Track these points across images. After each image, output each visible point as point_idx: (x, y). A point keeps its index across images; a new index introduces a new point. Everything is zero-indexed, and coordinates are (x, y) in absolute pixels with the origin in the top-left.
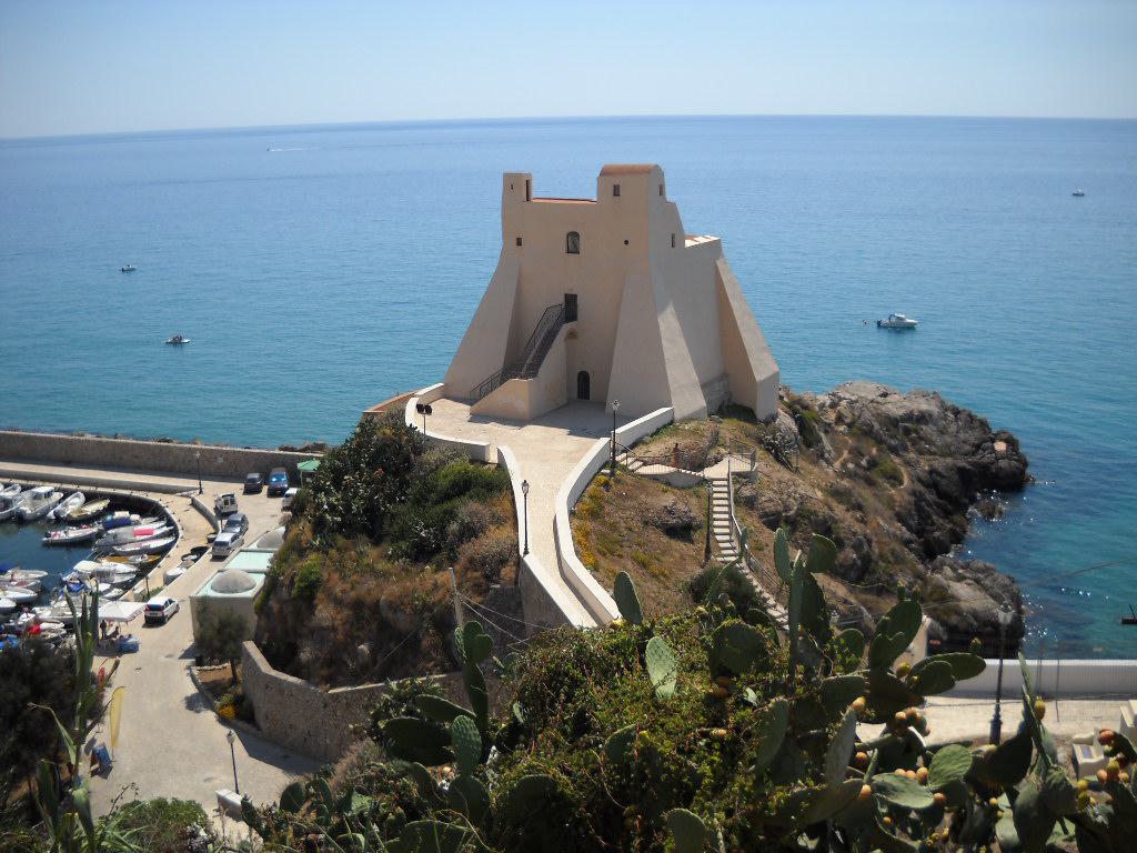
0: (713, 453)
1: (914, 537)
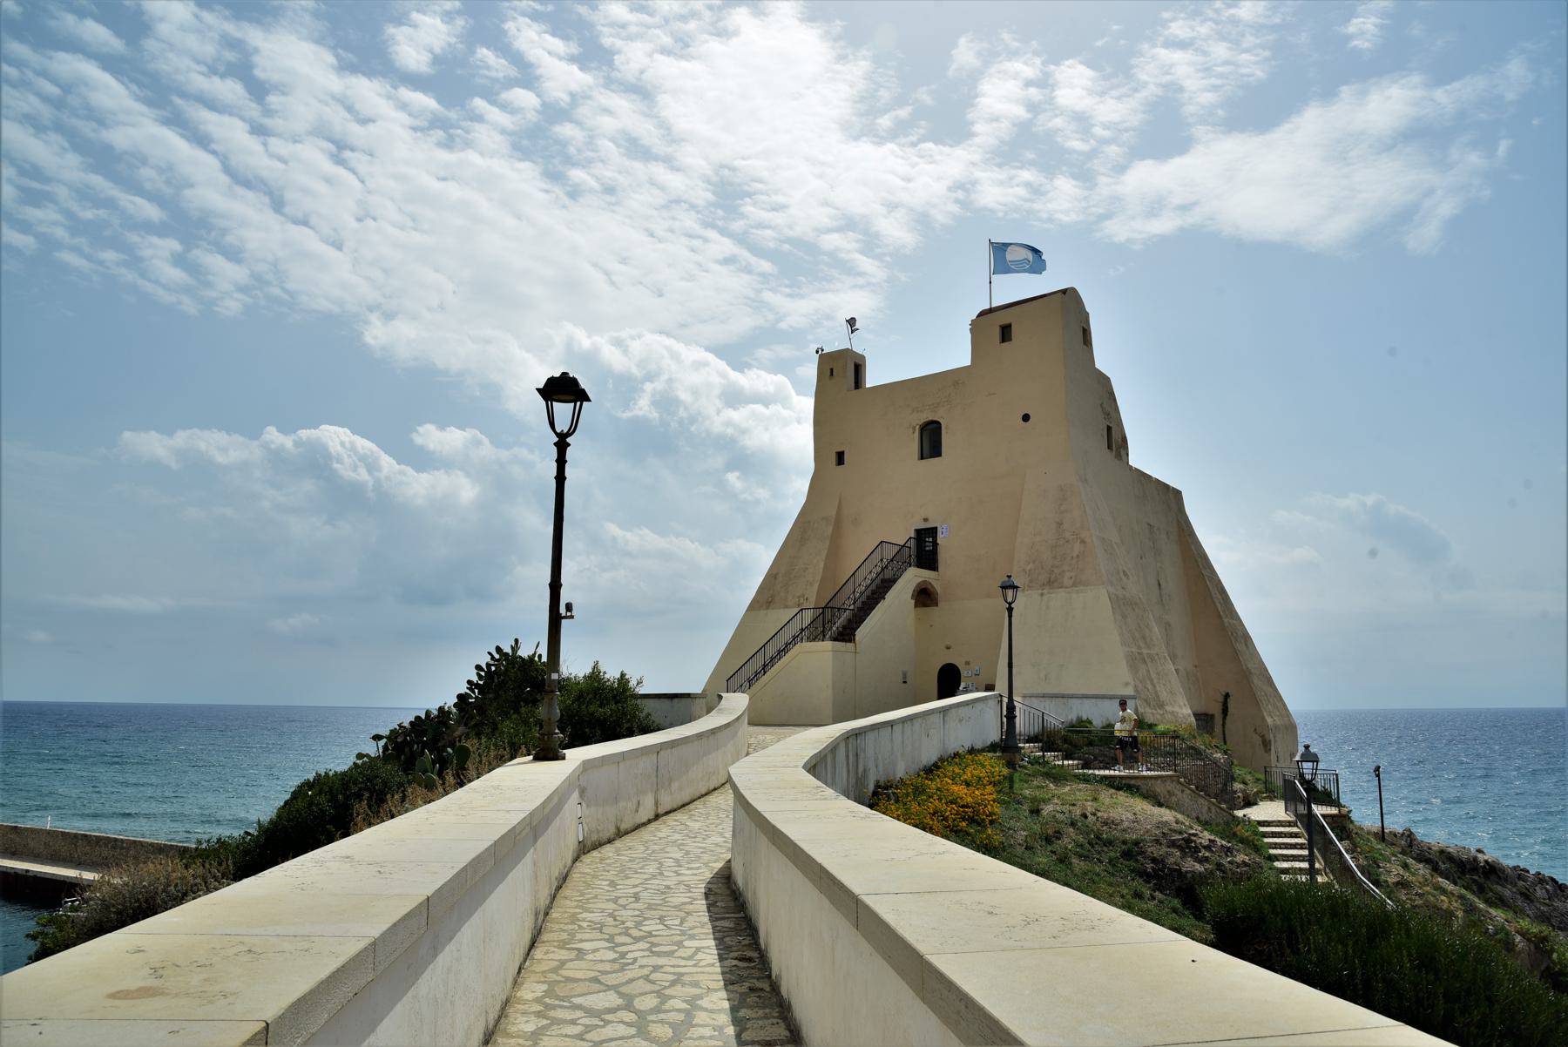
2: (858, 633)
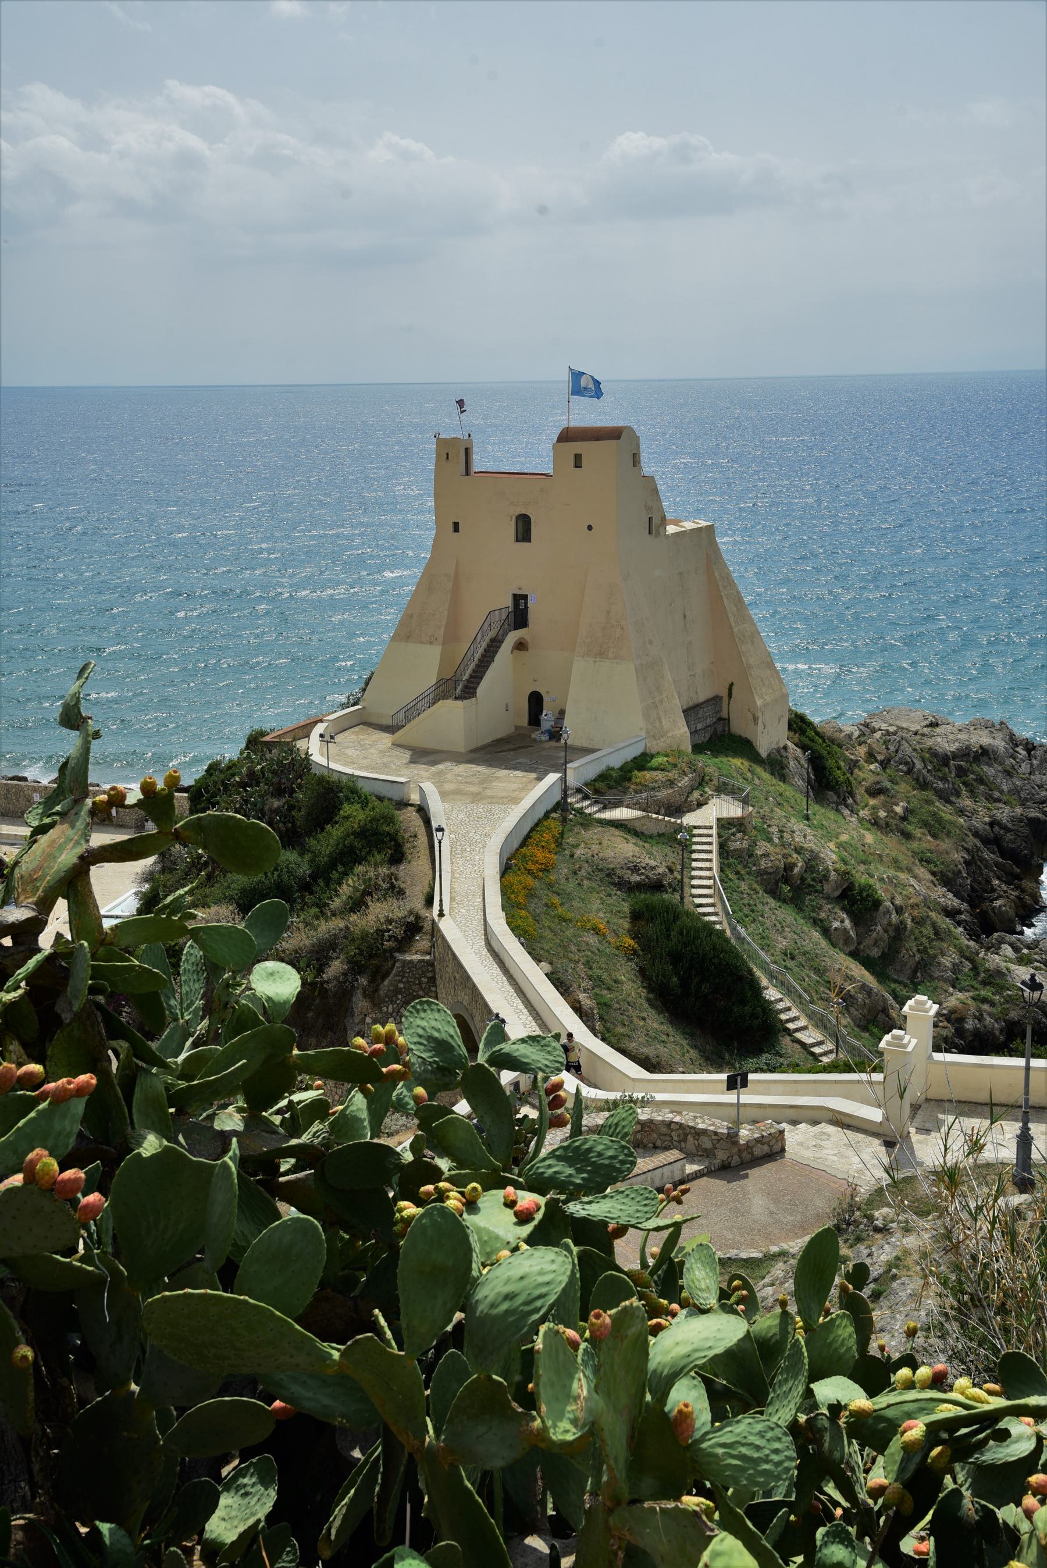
0: (696, 795)
1: (964, 906)
2: (478, 690)
